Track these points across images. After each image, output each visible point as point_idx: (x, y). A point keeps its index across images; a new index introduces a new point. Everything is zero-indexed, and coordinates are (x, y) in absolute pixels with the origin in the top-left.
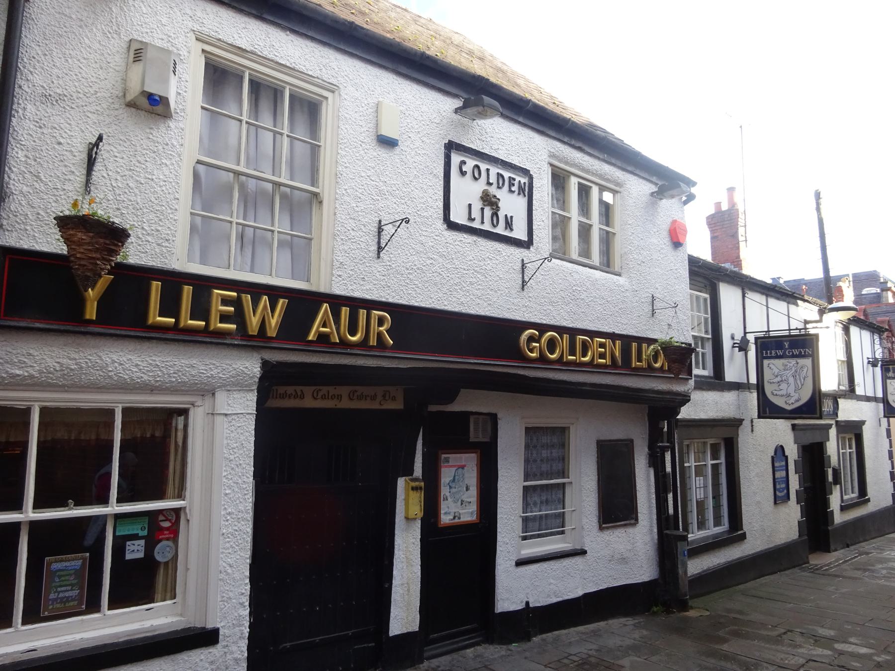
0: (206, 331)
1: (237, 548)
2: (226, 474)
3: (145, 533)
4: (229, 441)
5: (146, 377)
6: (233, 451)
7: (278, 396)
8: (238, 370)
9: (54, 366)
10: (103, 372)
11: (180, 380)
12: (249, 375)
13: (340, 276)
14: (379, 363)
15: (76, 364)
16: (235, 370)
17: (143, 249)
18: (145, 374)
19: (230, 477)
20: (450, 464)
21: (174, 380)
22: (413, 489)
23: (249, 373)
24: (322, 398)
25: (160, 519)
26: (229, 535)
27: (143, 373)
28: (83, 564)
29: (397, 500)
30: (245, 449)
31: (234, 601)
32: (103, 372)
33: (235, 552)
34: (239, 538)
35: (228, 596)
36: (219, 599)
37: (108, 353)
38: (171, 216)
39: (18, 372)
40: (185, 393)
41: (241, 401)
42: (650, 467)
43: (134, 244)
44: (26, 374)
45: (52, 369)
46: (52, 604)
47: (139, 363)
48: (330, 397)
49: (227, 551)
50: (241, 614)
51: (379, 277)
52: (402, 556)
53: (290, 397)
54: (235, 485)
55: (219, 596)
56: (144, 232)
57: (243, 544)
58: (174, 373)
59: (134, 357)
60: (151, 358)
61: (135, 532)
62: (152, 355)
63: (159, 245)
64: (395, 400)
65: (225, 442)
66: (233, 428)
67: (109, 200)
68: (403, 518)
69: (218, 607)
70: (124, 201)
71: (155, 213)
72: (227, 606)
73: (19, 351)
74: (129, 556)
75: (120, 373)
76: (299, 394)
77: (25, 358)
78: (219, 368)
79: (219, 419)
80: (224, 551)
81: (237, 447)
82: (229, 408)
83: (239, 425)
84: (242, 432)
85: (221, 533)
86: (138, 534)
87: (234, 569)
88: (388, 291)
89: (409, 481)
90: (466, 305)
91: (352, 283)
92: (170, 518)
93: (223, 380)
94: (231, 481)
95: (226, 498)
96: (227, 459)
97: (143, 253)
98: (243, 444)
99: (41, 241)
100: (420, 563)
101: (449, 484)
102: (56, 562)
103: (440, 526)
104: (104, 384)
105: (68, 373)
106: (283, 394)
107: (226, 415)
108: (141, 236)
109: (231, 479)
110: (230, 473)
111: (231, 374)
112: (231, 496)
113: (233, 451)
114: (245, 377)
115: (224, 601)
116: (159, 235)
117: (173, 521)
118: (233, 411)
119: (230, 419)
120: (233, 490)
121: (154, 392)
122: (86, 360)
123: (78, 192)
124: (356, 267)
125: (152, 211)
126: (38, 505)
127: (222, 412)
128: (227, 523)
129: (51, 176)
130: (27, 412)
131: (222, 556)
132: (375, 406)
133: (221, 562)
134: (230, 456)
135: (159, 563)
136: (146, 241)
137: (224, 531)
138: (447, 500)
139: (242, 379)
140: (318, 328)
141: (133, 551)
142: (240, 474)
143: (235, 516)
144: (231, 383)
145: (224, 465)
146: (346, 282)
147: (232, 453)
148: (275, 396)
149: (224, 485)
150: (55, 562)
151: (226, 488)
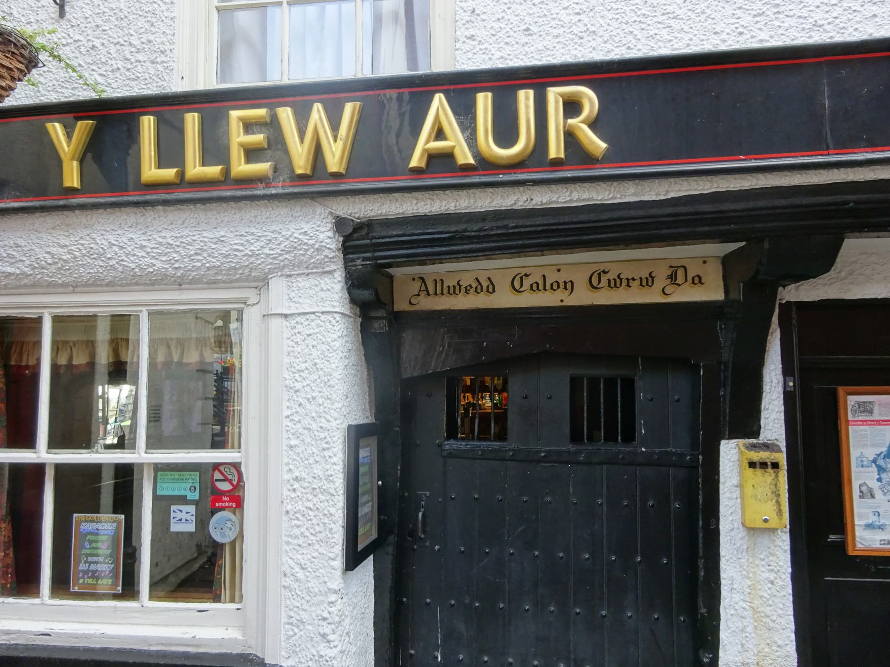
0: (226, 179)
1: (312, 538)
2: (289, 412)
3: (196, 496)
4: (293, 359)
5: (159, 264)
6: (301, 376)
7: (445, 291)
8: (291, 239)
9: (44, 257)
10: (103, 261)
11: (207, 265)
12: (313, 246)
13: (471, 37)
14: (586, 196)
15: (69, 253)
16: (287, 239)
17: (134, 74)
18: (157, 259)
19: (296, 418)
20: (876, 416)
21: (200, 264)
22: (752, 465)
23: (311, 242)
24: (531, 289)
25: (216, 477)
26: (298, 515)
27: (154, 257)
28: (118, 527)
29: (721, 487)
30: (321, 372)
31: (310, 627)
32: (103, 261)
33: (309, 545)
34: (315, 521)
35: (299, 618)
36: (284, 620)
37: (104, 232)
38: (166, 14)
39: (9, 270)
40: (227, 285)
41: (312, 292)
42: (74, 212)
43: (122, 70)
44: (18, 272)
45: (43, 263)
46: (83, 577)
47: (144, 243)
48: (548, 286)
49: (295, 541)
50: (322, 653)
51: (566, 19)
52: (742, 604)
53: (467, 291)
54: (306, 432)
55: (283, 614)
56: (133, 50)
57: (323, 534)
58: (197, 254)
59: (137, 236)
60: (160, 234)
61: (182, 493)
62: (160, 229)
63: (153, 62)
64: (700, 282)
65: (287, 360)
66: (299, 338)
67: (87, 18)
68: (737, 524)
69: (283, 632)
70: (104, 12)
71: (145, 17)
72: (299, 634)
73: (6, 243)
74: (175, 528)
75: (122, 260)
76: (485, 284)
77: (14, 250)
78: (262, 239)
79: (275, 323)
80: (290, 540)
81: (307, 369)
82: (291, 304)
83: (308, 332)
84: (315, 343)
85: (284, 510)
86: (186, 496)
87: (308, 574)
88: (593, 43)
89: (743, 449)
90: (827, 27)
91: (502, 44)
92: (230, 477)
93: (274, 258)
94: (299, 426)
95: (291, 452)
96: (291, 388)
97: (134, 80)
98: (316, 364)
99: (20, 96)
100: (793, 627)
101: (874, 461)
102: (86, 521)
103: (851, 553)
104: (110, 278)
105: (63, 266)
106: (454, 287)
107: (286, 316)
108: (128, 56)
109: (299, 421)
110: (297, 412)
111: (282, 247)
112: (299, 450)
113: (301, 376)
114: (307, 250)
115: (291, 624)
116: (152, 48)
117: (235, 483)
118: (297, 309)
119: (293, 322)
120: (303, 440)
121: (183, 286)
122: (79, 246)
123: (53, 19)
124: (509, 12)
125: (140, 16)
126: (54, 443)
127: (278, 312)
128: (293, 495)
129: (24, 9)
130: (39, 320)
131: (287, 548)
132: (652, 297)
133: (285, 558)
134: (296, 384)
135: (221, 546)
136: (137, 61)
137: (289, 507)
138: (873, 496)
139: (303, 255)
140: (427, 142)
141: (181, 520)
142: (314, 415)
143: (307, 484)
144: (286, 262)
145: (286, 398)
146: (486, 45)
147: (299, 379)
148: (439, 292)
149: (287, 431)
150: (84, 522)
151: (290, 436)
